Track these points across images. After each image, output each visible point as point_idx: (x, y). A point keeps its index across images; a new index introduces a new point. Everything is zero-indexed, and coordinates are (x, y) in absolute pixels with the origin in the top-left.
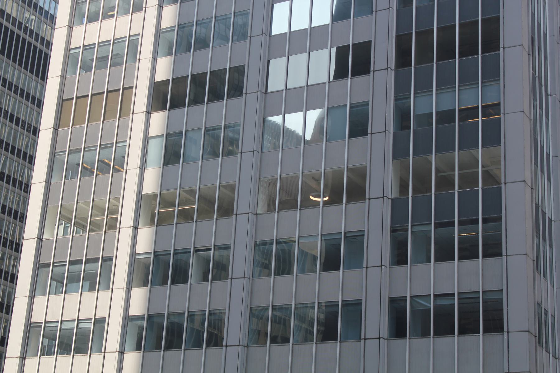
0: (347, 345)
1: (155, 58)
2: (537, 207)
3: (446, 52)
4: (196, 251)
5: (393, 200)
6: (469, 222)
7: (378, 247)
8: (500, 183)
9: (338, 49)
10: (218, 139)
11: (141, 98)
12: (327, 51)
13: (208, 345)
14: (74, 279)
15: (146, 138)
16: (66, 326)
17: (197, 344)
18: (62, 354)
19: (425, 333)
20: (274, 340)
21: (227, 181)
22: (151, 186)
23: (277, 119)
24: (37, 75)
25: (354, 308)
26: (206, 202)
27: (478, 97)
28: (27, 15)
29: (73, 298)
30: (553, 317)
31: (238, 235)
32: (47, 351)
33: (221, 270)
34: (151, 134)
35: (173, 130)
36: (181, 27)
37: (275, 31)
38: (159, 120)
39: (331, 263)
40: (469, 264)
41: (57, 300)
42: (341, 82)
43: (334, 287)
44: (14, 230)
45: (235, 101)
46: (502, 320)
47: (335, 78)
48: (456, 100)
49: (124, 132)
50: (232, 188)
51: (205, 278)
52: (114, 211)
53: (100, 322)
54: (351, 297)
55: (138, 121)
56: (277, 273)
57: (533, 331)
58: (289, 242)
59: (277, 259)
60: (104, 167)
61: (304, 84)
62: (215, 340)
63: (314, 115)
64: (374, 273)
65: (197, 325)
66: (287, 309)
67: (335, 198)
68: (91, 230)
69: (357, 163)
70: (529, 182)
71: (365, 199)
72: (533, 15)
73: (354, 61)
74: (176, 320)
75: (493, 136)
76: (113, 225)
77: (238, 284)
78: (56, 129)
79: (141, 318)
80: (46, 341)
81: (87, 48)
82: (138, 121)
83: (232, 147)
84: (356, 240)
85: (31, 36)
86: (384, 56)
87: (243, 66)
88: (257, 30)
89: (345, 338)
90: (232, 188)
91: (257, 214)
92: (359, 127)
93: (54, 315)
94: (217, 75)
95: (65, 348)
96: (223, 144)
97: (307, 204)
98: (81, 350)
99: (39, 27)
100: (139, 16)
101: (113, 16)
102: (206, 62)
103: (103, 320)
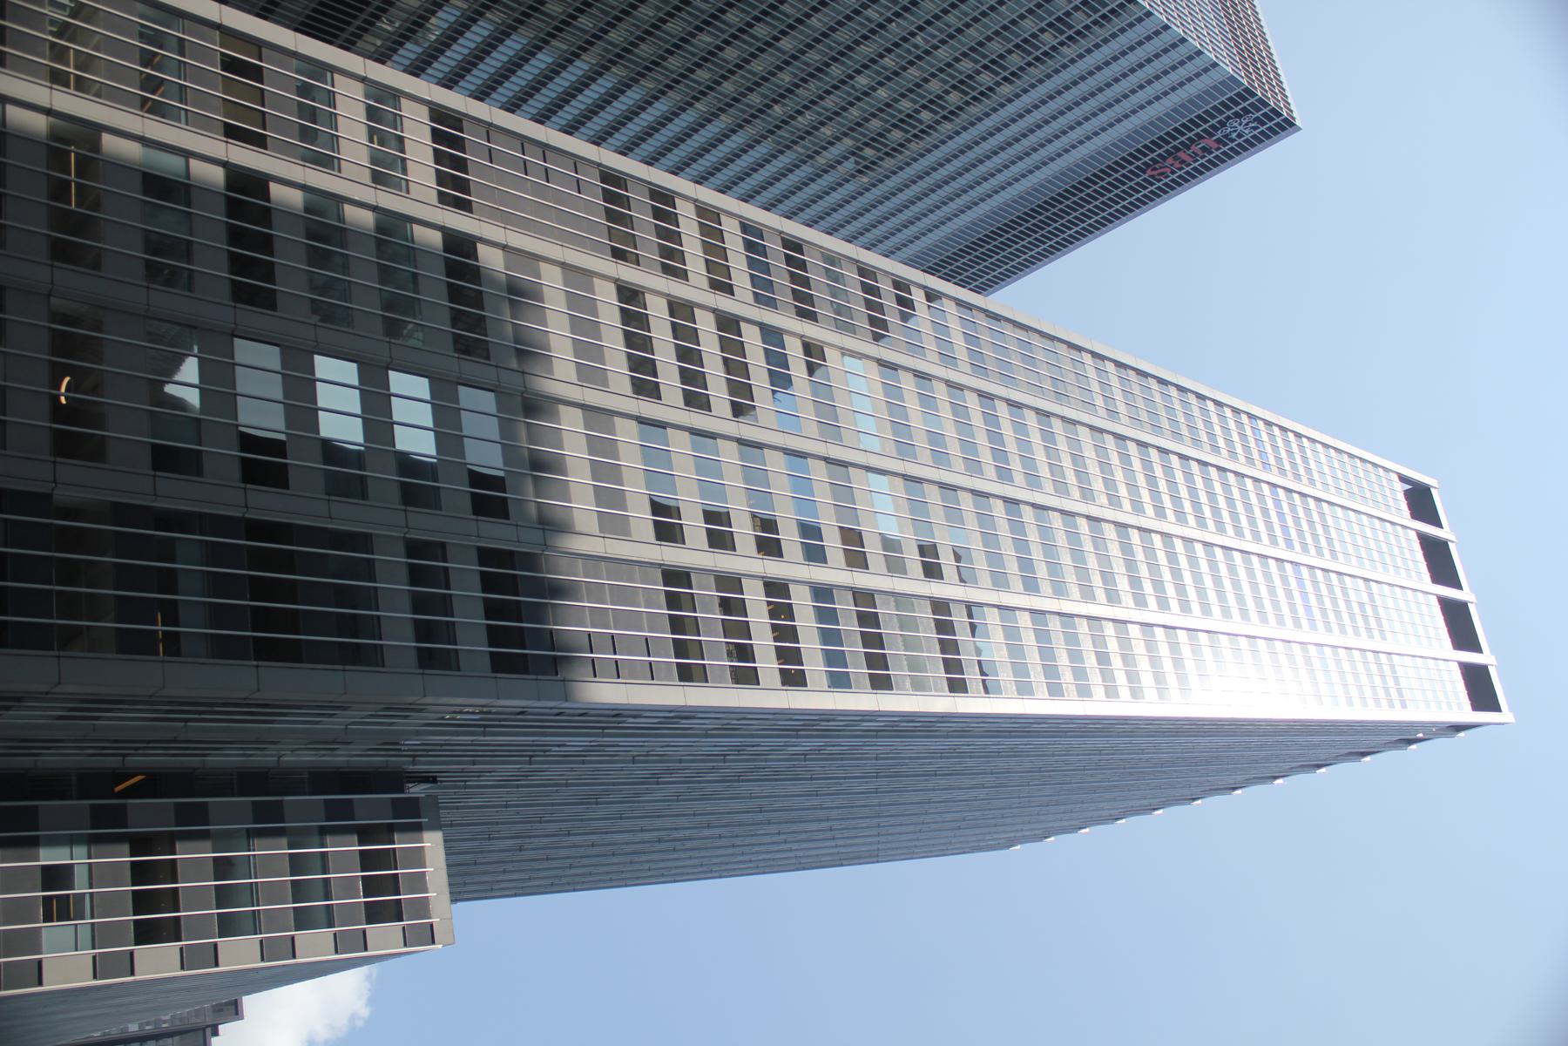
2: (19, 699)
5: (49, 497)
11: (69, 102)
12: (282, 427)
15: (187, 154)
34: (193, 163)
37: (319, 360)
38: (217, 175)
46: (369, 665)
47: (471, 472)
49: (203, 124)
50: (96, 266)
52: (82, 86)
61: (239, 389)
63: (193, 397)
68: (53, 45)
70: (56, 690)
71: (328, 494)
72: (121, 702)
73: (263, 462)
75: (132, 645)
76: (58, 78)
78: (218, 27)
81: (331, 99)
86: (266, 504)
90: (96, 266)
91: (49, 295)
92: (165, 460)
100: (366, 177)
101: (371, 141)
102: (289, 260)
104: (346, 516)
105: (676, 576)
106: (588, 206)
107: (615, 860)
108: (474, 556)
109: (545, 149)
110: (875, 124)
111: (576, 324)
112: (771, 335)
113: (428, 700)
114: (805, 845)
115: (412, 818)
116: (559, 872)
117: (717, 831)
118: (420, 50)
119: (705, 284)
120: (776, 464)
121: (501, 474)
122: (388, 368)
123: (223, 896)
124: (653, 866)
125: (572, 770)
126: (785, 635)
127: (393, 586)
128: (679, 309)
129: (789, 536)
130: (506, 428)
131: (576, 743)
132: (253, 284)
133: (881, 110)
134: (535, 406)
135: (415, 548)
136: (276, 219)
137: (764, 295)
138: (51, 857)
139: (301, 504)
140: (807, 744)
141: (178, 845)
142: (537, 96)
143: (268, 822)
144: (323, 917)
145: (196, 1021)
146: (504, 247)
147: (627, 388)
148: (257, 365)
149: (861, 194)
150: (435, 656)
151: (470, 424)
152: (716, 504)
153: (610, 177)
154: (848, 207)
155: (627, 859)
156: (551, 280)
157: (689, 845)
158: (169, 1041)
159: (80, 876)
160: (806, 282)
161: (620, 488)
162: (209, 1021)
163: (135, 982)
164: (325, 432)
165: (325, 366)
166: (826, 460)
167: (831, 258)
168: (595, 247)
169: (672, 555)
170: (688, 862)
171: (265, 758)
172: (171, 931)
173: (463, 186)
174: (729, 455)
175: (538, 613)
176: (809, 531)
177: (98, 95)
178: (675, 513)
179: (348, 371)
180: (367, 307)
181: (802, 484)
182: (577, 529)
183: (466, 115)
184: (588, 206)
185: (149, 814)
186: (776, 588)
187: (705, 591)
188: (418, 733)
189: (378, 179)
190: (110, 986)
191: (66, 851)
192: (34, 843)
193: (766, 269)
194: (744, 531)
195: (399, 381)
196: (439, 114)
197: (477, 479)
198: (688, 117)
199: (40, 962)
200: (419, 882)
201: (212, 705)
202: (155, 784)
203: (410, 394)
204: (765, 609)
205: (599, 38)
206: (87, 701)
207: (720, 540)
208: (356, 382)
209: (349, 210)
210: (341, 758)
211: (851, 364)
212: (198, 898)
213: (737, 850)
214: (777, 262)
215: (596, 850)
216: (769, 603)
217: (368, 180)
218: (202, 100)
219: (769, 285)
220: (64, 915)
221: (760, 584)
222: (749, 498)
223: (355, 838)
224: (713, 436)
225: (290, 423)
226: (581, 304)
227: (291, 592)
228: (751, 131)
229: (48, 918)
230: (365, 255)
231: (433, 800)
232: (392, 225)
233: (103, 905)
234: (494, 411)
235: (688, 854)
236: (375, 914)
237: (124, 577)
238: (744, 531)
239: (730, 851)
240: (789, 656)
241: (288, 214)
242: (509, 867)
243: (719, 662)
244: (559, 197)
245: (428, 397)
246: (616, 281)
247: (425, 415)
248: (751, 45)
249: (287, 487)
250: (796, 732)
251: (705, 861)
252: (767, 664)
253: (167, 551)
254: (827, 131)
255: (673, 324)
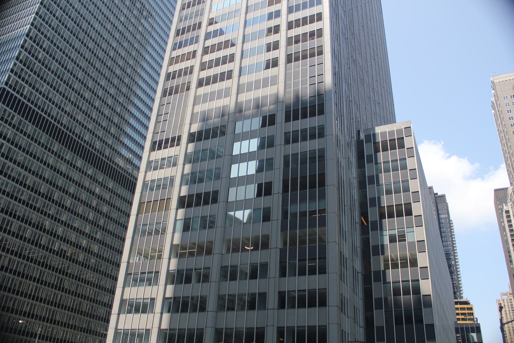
0: (260, 312)
1: (181, 186)
2: (341, 253)
3: (303, 187)
4: (195, 269)
5: (280, 249)
6: (312, 259)
7: (274, 269)
8: (325, 243)
9: (258, 185)
10: (206, 221)
11: (174, 203)
12: (253, 185)
13: (199, 311)
14: (142, 280)
15: (176, 220)
16: (138, 301)
17: (195, 310)
18: (136, 313)
19: (294, 307)
20: (228, 309)
21: (210, 240)
22: (176, 241)
23: (232, 213)
24: (131, 192)
25: (263, 296)
26: (200, 249)
27: (317, 207)
28: (128, 166)
29: (142, 289)
30: (347, 300)
31: (214, 263)
32: (129, 312)
33: (206, 278)
35: (187, 217)
36: (192, 173)
37: (232, 176)
38: (181, 211)
39: (253, 276)
40: (312, 277)
41: (135, 289)
42: (259, 198)
43: (255, 286)
44: (118, 258)
45: (214, 205)
48: (308, 207)
49: (166, 216)
50: (212, 242)
51: (199, 281)
52: (160, 251)
53: (153, 300)
54: (262, 291)
55: (172, 213)
56: (230, 280)
57: (339, 306)
58: (236, 266)
59: (227, 304)
60: (157, 232)
62: (203, 309)
63: (247, 212)
64: (272, 281)
65: (195, 302)
66: (234, 296)
67: (256, 248)
68: (150, 259)
69: (265, 233)
70: (337, 242)
73: (264, 190)
74: (186, 299)
75: (323, 222)
76: (160, 257)
77: (213, 285)
78: (137, 215)
79: (171, 298)
80: (129, 307)
81: (153, 181)
82: (172, 213)
83: (212, 224)
84: (265, 266)
85: (129, 175)
86: (277, 187)
87: (218, 191)
88: (224, 175)
89: (259, 309)
90: (212, 242)
92: (267, 218)
93: (133, 296)
94: (207, 194)
95: (137, 311)
96: (208, 223)
97: (244, 250)
98: (144, 311)
99: (132, 172)
100: (175, 168)
101: (164, 168)
103: (154, 299)
104: (279, 164)
105: (289, 59)
106: (174, 100)
107: (381, 73)
109: (159, 115)
110: (135, 12)
111: (212, 99)
112: (208, 36)
114: (374, 11)
115: (371, 137)
116: (386, 91)
117: (371, 40)
118: (135, 159)
119: (194, 60)
120: (249, 30)
121: (261, 117)
122: (232, 155)
123: (397, 191)
124: (382, 61)
126: (304, 21)
127: (299, 147)
128: (203, 67)
129: (273, 23)
130: (246, 118)
131: (344, 87)
132: (210, 198)
133: (130, 11)
134: (239, 110)
135: (287, 142)
136: (191, 193)
137: (195, 40)
138: (386, 241)
140: (341, 11)
141: (382, 205)
142: (139, 141)
143: (374, 180)
144: (403, 162)
146: (191, 124)
147: (230, 81)
148: (236, 194)
149: (158, 14)
150: (320, 133)
151: (246, 129)
152: (265, 48)
153: (164, 94)
154: (161, 35)
155: (381, 70)
156: (198, 109)
157: (375, 50)
159: (392, 232)
160: (189, 27)
161: (263, 81)
164: (255, 149)
166: (246, 13)
167: (180, 20)
168: (187, 96)
169: (282, 61)
170: (381, 50)
171: (355, 183)
172: (408, 205)
173: (173, 139)
174: (248, 46)
175: (304, 103)
176: (270, 17)
178: (268, 62)
180: (213, 164)
181: (255, 21)
182: (276, 92)
184: (174, 100)
185: (373, 214)
186: (290, 26)
187: (293, 49)
188: (345, 136)
189: (175, 165)
190: (425, 222)
191: (385, 237)
192: (383, 246)
193: (186, 41)
194: (272, 38)
195: (236, 152)
196: (153, 149)
198: (143, 74)
199: (418, 241)
200: (391, 133)
201: (339, 199)
202: (364, 214)
204: (297, 29)
205: (122, 104)
206: (340, 234)
207: (276, 46)
209: (186, 172)
210: (354, 160)
211: (214, 9)
212: (396, 176)
213: (376, 34)
214: (184, 37)
215: (378, 80)
216: (295, 28)
218: (159, 218)
219: (192, 39)
221: (289, 31)
222: (261, 38)
224: (242, 52)
226: (206, 98)
227: (304, 178)
228: (144, 53)
229: (405, 240)
230: (199, 166)
231: (366, 130)
232: (188, 159)
233: (401, 224)
234: (242, 122)
235: (378, 50)
238: (272, 38)
239: (377, 36)
240: (312, 19)
242: (385, 107)
243: (316, 42)
244: (173, 109)
246: (197, 88)
247: (245, 143)
248: (116, 56)
250: (337, 15)
251: (380, 44)
252: (315, 26)
253: (294, 215)
254: (140, 29)
255: (208, 69)
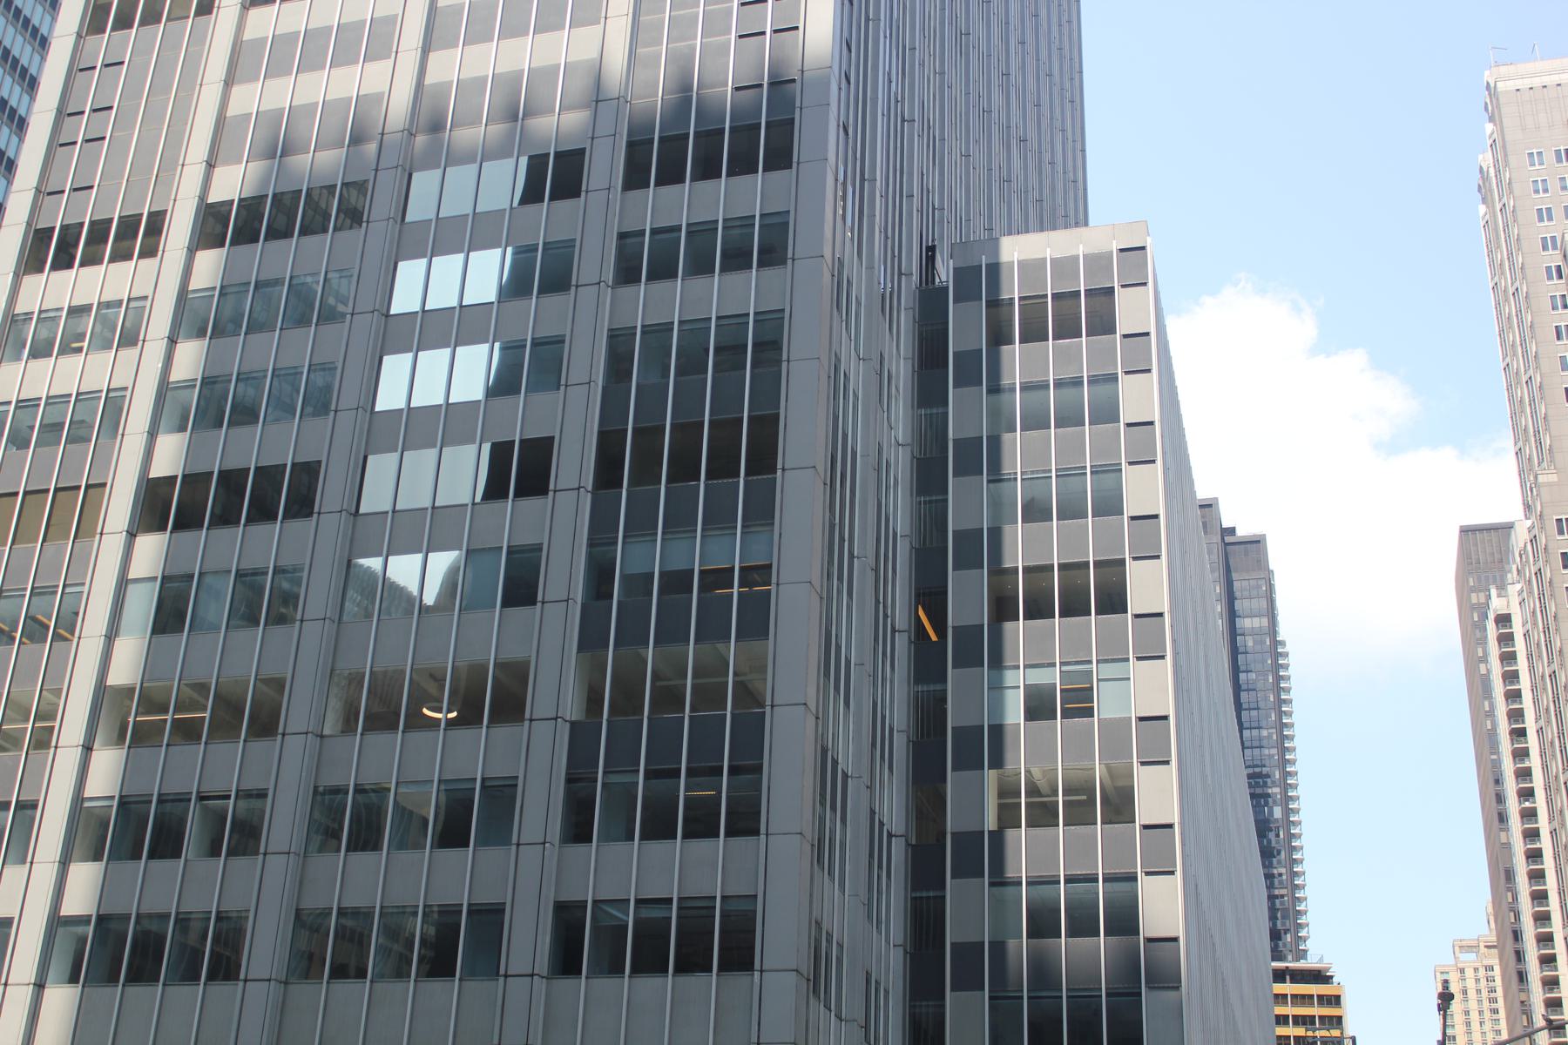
2: (824, 751)
5: (574, 725)
12: (473, 448)
15: (123, 583)
50: (278, 684)
63: (442, 562)
73: (521, 470)
75: (757, 622)
76: (43, 741)
86: (574, 465)
91: (322, 736)
92: (522, 588)
100: (130, 354)
101: (80, 350)
102: (250, 449)
104: (587, 363)
108: (635, 194)
109: (64, 113)
111: (310, 63)
113: (827, 253)
115: (979, 279)
116: (1056, 90)
122: (387, 315)
125: (922, 65)
132: (284, 493)
134: (430, 119)
135: (627, 273)
138: (1015, 711)
139: (572, 422)
143: (981, 456)
144: (1103, 389)
145: (1217, 556)
148: (387, 483)
150: (771, 244)
158: (1236, 585)
159: (1039, 677)
162: (1217, 538)
163: (1171, 612)
164: (477, 393)
165: (390, 397)
171: (901, 464)
172: (1113, 570)
177: (58, 692)
179: (395, 367)
180: (301, 348)
182: (595, 55)
183: (29, 224)
185: (966, 598)
188: (870, 267)
189: (130, 338)
190: (1174, 641)
191: (1009, 694)
192: (998, 731)
195: (405, 300)
197: (532, 194)
200: (1065, 266)
201: (832, 526)
202: (931, 596)
203: (422, 284)
206: (827, 674)
208: (409, 356)
210: (902, 369)
215: (1029, 38)
217: (135, 351)
220: (1085, 694)
223: (1005, 348)
225: (467, 439)
229: (1089, 712)
232: (190, 317)
236: (1103, 324)
237: (671, 633)
241: (129, 771)
242: (1047, 157)
244: (131, 92)
245: (424, 261)
249: (552, 439)
